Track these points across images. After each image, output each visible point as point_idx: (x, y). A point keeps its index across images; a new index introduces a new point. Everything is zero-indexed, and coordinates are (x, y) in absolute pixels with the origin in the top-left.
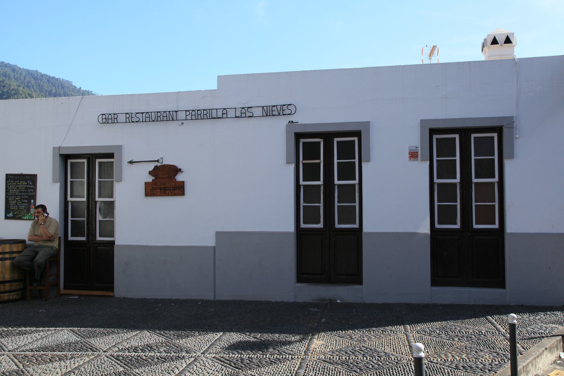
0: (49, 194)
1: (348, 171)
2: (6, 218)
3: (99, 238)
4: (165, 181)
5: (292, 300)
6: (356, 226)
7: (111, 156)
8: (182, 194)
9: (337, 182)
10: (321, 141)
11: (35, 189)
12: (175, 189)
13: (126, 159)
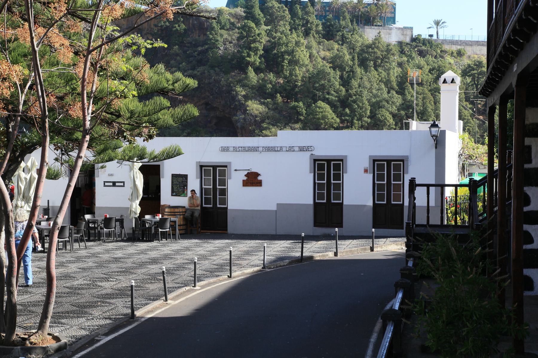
0: (194, 184)
1: (338, 177)
2: (172, 195)
3: (218, 206)
4: (252, 180)
5: (312, 234)
6: (341, 202)
7: (226, 166)
8: (261, 185)
9: (332, 182)
10: (326, 163)
11: (187, 182)
12: (257, 183)
13: (233, 168)
